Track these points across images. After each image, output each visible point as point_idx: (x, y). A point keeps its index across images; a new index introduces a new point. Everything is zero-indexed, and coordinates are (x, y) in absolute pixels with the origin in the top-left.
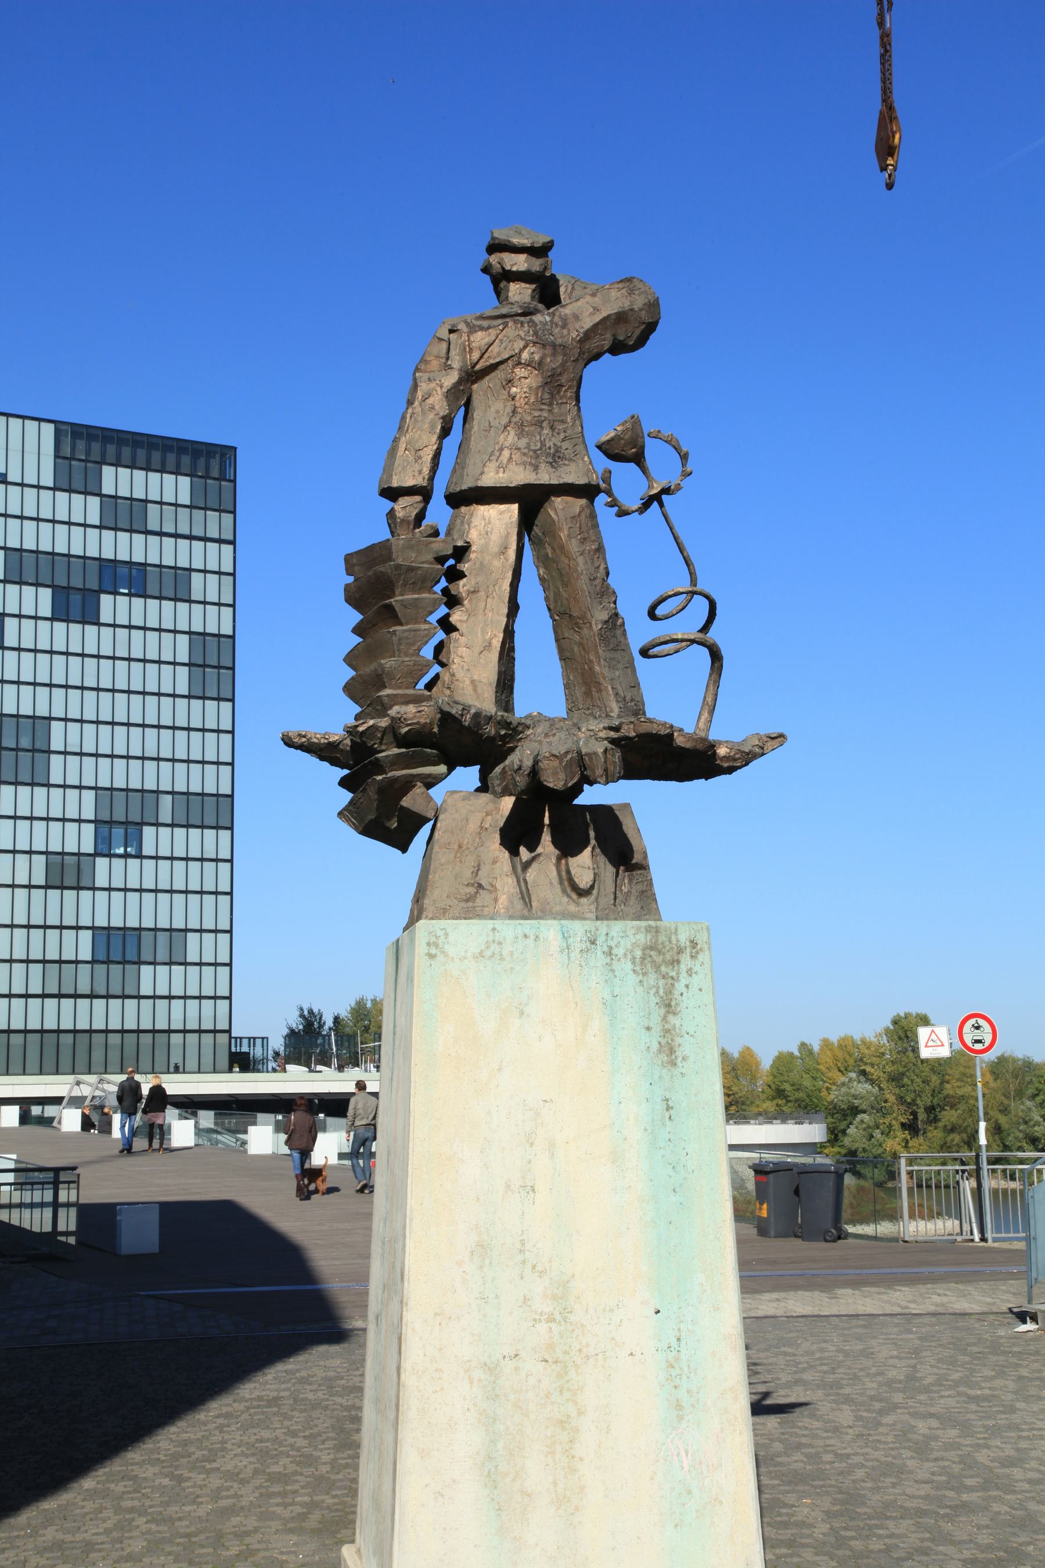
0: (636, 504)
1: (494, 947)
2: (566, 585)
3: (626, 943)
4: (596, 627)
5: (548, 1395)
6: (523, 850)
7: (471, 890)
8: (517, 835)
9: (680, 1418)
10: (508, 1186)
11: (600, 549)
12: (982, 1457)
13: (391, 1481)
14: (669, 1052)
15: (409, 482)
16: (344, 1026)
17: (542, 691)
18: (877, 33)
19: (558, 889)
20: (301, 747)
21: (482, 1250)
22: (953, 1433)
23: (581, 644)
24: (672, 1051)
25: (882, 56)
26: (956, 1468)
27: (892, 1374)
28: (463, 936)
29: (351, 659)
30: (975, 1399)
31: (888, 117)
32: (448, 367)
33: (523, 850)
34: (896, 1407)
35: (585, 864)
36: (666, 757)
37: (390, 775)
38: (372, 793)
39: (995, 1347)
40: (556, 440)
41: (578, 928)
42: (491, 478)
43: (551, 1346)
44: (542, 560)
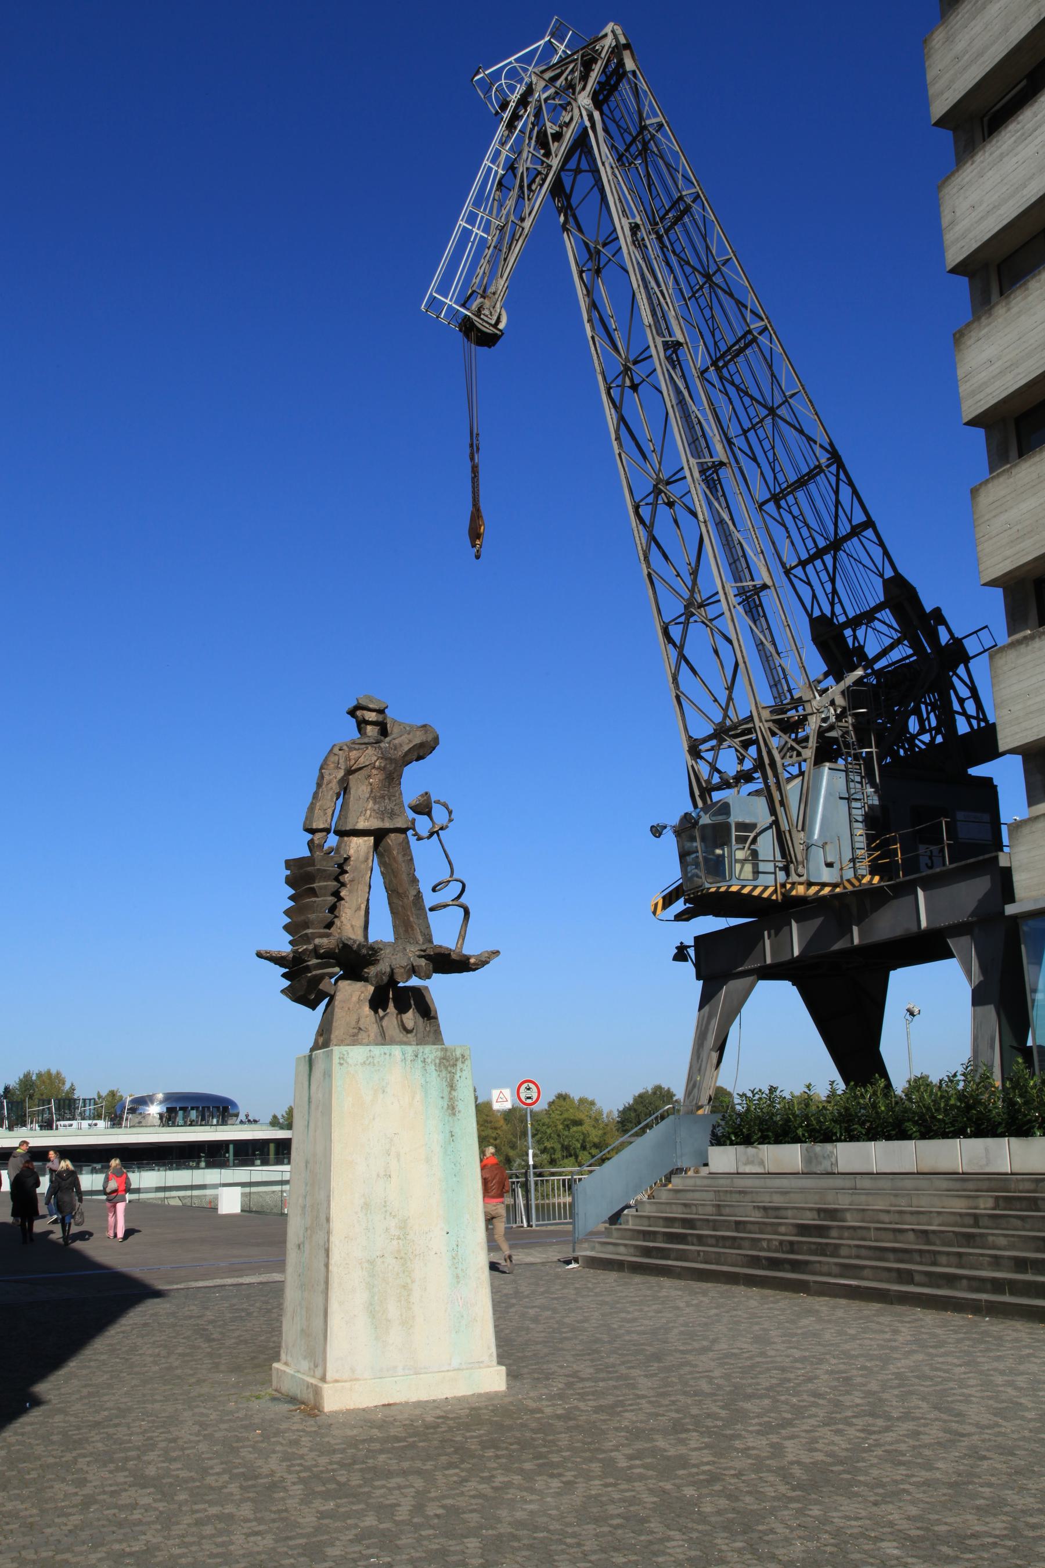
0: (426, 834)
1: (370, 1059)
2: (395, 877)
3: (432, 1056)
4: (411, 898)
5: (398, 1274)
6: (380, 1011)
7: (356, 1031)
8: (377, 1003)
9: (458, 1282)
10: (378, 1175)
11: (412, 859)
12: (567, 1320)
13: (322, 1317)
14: (452, 1109)
15: (321, 826)
16: (13, 1095)
17: (382, 930)
18: (469, 465)
19: (397, 1030)
20: (266, 958)
21: (366, 1206)
22: (549, 1313)
23: (403, 907)
24: (453, 1108)
25: (473, 478)
26: (556, 1326)
27: (505, 1291)
28: (356, 1053)
29: (288, 913)
30: (556, 1299)
31: (476, 516)
32: (338, 768)
33: (380, 1011)
34: (513, 1305)
35: (410, 1017)
36: (448, 963)
37: (314, 973)
38: (304, 982)
39: (558, 1276)
40: (392, 805)
41: (410, 1049)
42: (362, 825)
43: (399, 1251)
44: (382, 863)
